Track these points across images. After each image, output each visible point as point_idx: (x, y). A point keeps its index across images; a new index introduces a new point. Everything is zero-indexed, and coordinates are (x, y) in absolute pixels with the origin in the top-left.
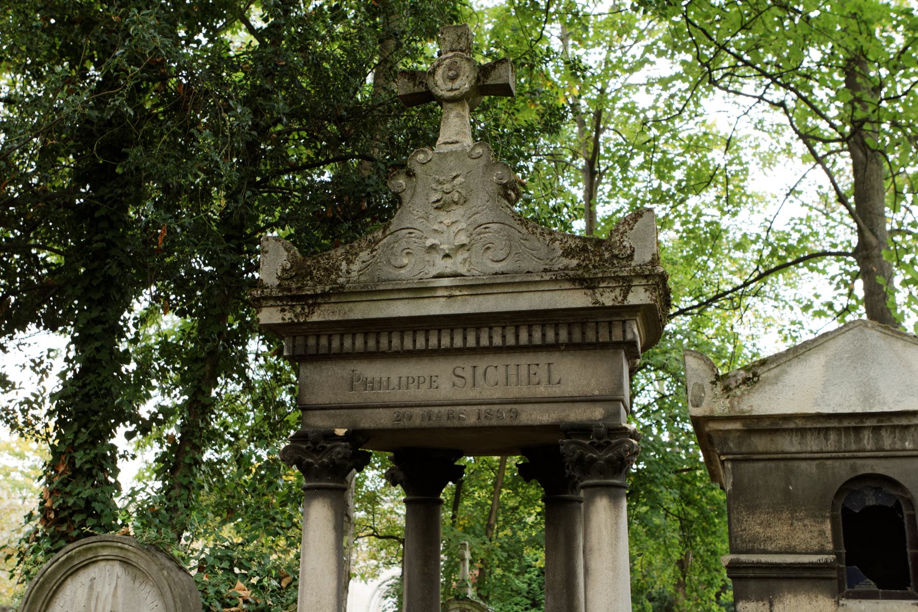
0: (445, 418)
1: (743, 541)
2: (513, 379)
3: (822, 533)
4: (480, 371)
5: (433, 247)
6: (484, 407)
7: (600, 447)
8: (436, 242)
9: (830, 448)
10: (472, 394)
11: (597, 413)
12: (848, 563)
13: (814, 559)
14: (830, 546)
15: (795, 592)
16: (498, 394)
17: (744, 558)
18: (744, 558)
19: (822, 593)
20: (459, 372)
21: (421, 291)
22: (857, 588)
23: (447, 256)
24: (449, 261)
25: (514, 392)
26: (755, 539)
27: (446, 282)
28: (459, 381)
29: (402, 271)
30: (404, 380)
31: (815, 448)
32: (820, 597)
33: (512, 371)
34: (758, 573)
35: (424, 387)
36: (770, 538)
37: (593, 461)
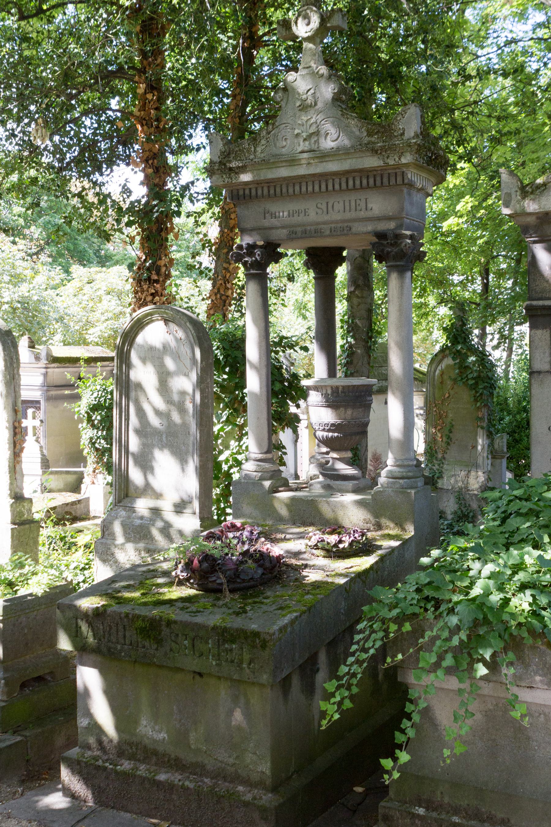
1: (536, 292)
2: (347, 208)
4: (330, 205)
5: (298, 135)
6: (333, 226)
8: (300, 131)
10: (326, 218)
11: (392, 225)
16: (338, 217)
17: (535, 303)
18: (535, 303)
20: (319, 205)
21: (292, 162)
23: (305, 140)
24: (307, 143)
25: (348, 215)
27: (305, 155)
28: (319, 211)
33: (347, 204)
34: (545, 312)
35: (302, 215)
37: (388, 253)
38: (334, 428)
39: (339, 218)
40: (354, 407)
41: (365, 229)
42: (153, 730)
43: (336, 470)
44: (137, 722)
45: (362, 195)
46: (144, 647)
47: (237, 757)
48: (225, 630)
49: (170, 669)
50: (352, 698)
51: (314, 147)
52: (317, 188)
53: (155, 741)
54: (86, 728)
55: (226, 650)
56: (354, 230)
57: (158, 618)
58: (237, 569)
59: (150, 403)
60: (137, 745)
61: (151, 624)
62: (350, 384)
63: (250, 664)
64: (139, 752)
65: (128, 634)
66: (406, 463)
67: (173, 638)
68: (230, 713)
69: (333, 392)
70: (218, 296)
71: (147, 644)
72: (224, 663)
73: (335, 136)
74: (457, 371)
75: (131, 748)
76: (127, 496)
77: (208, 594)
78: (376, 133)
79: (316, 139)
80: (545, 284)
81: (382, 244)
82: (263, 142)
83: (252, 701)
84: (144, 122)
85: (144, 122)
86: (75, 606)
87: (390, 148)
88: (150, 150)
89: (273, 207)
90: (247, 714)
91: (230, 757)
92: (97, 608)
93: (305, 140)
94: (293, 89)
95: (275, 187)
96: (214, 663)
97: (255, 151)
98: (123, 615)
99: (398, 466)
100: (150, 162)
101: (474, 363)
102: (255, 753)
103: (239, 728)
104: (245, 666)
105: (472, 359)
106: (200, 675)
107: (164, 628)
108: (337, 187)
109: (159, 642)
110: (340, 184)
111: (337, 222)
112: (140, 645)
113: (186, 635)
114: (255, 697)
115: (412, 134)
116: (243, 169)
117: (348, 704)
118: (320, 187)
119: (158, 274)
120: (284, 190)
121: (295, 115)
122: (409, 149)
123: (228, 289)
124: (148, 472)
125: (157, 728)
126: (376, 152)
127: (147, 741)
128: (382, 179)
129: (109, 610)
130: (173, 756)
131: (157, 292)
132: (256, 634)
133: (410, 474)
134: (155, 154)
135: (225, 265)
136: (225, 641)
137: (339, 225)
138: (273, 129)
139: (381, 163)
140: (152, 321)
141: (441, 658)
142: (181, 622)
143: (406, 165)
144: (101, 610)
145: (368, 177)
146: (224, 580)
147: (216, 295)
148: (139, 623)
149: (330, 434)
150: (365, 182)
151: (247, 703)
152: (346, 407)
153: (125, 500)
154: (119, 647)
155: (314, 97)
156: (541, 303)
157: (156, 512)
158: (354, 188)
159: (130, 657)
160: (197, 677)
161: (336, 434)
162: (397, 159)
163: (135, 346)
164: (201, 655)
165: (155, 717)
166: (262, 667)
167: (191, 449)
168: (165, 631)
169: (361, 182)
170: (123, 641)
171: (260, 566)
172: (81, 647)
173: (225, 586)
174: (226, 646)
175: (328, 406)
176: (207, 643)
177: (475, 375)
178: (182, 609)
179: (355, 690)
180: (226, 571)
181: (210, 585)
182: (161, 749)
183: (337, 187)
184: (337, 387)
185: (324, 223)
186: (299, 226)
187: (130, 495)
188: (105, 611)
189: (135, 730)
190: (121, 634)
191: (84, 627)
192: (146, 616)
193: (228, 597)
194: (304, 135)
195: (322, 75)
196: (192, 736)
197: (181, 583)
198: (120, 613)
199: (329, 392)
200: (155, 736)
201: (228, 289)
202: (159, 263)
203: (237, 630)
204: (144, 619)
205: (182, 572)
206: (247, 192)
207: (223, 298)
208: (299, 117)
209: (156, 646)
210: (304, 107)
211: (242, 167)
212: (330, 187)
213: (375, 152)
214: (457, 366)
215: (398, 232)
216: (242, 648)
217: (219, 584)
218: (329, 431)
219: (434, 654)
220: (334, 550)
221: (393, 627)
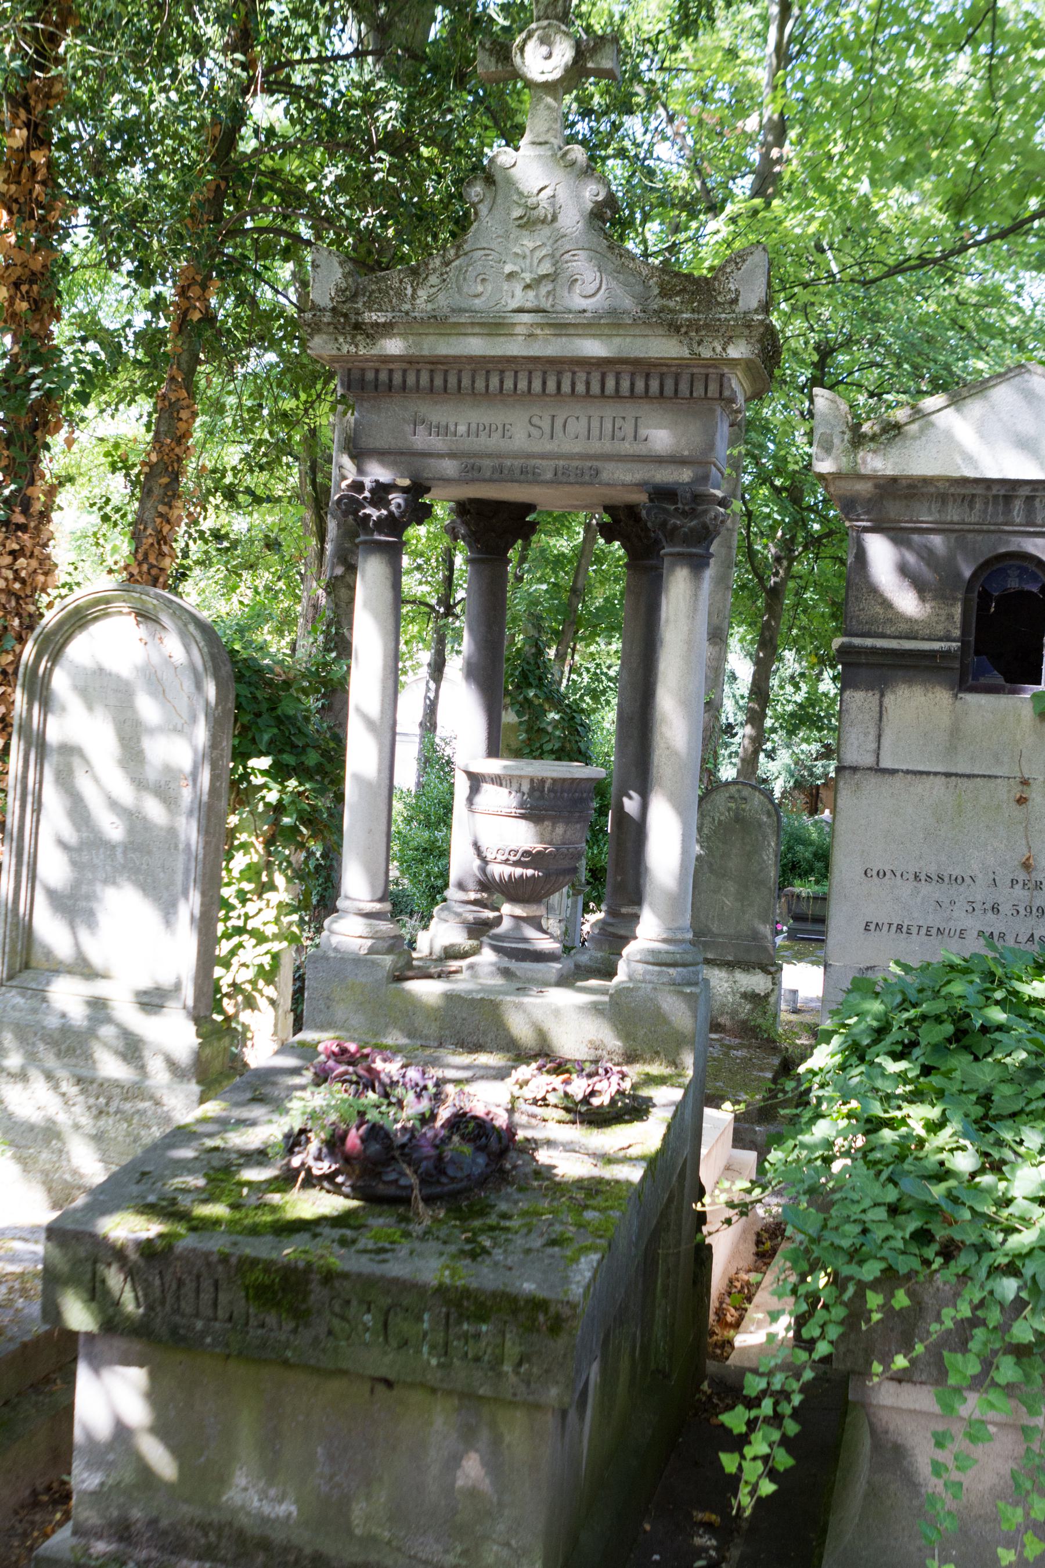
0: (517, 472)
1: (859, 622)
2: (595, 432)
3: (950, 617)
5: (511, 275)
6: (561, 463)
7: (684, 514)
8: (516, 269)
9: (973, 519)
10: (549, 447)
11: (685, 475)
12: (977, 653)
13: (936, 646)
14: (957, 633)
15: (910, 682)
16: (577, 448)
17: (857, 641)
18: (857, 641)
19: (940, 683)
20: (536, 420)
22: (983, 680)
23: (528, 287)
24: (531, 294)
25: (596, 446)
26: (873, 620)
27: (526, 318)
28: (535, 432)
29: (477, 301)
30: (474, 426)
31: (956, 518)
32: (938, 689)
33: (595, 424)
35: (496, 436)
36: (890, 620)
37: (675, 528)
38: (530, 859)
39: (576, 450)
40: (568, 822)
41: (628, 478)
42: (263, 1495)
43: (526, 940)
44: (223, 1480)
45: (629, 410)
46: (262, 1325)
47: (465, 1553)
48: (466, 1293)
49: (316, 1371)
50: (785, 1442)
51: (547, 304)
52: (537, 385)
53: (265, 1520)
54: (93, 1493)
55: (465, 1337)
56: (605, 476)
57: (301, 1265)
58: (440, 1158)
59: (96, 780)
60: (220, 1529)
61: (285, 1279)
62: (568, 776)
63: (520, 1364)
64: (224, 1542)
65: (223, 1298)
66: (679, 936)
67: (337, 1309)
68: (454, 1462)
69: (532, 789)
70: (145, 567)
71: (271, 1319)
72: (457, 1362)
73: (591, 288)
74: (523, 736)
75: (206, 1535)
76: (26, 966)
77: (377, 1209)
78: (678, 293)
79: (550, 287)
80: (878, 609)
81: (666, 511)
82: (433, 279)
83: (507, 1439)
84: (15, 207)
85: (15, 207)
86: (93, 1236)
87: (707, 326)
88: (24, 265)
89: (439, 413)
90: (494, 1465)
91: (446, 1551)
92: (149, 1241)
93: (528, 287)
94: (510, 182)
95: (446, 372)
96: (434, 1362)
97: (414, 297)
98: (214, 1258)
99: (665, 941)
100: (24, 288)
101: (556, 724)
102: (508, 1544)
103: (472, 1493)
104: (507, 1368)
105: (553, 716)
106: (389, 1384)
107: (315, 1286)
108: (581, 388)
109: (301, 1316)
110: (588, 384)
111: (570, 457)
112: (253, 1322)
113: (369, 1304)
114: (516, 1433)
115: (755, 304)
116: (386, 329)
117: (784, 1460)
118: (544, 383)
119: (25, 512)
120: (466, 382)
121: (506, 235)
122: (746, 332)
123: (164, 555)
124: (78, 920)
125: (272, 1492)
126: (677, 329)
127: (243, 1520)
128: (676, 384)
129: (180, 1246)
130: (308, 1551)
131: (22, 549)
132: (538, 1305)
133: (689, 958)
134: (33, 274)
135: (162, 509)
136: (462, 1317)
137: (575, 463)
138: (457, 256)
139: (685, 353)
140: (107, 615)
141: (988, 1364)
142: (359, 1275)
143: (733, 362)
144: (160, 1245)
145: (647, 376)
146: (414, 1180)
147: (140, 564)
148: (257, 1276)
149: (518, 871)
150: (640, 385)
151: (497, 1441)
152: (555, 820)
153: (25, 975)
154: (199, 1325)
155: (553, 204)
156: (869, 642)
157: (98, 1006)
158: (617, 395)
159: (227, 1345)
160: (380, 1388)
161: (530, 872)
162: (719, 349)
163: (64, 661)
164: (404, 1343)
165: (271, 1471)
166: (547, 1371)
167: (179, 878)
168: (317, 1293)
169: (632, 385)
170: (209, 1313)
171: (480, 1149)
172: (112, 1323)
173: (416, 1192)
174: (465, 1326)
175: (522, 817)
176: (419, 1319)
177: (557, 746)
178: (343, 1242)
179: (792, 1428)
180: (421, 1160)
181: (382, 1189)
182: (278, 1536)
183: (581, 388)
184: (543, 781)
185: (543, 456)
186: (489, 456)
187: (33, 964)
188: (170, 1247)
189: (219, 1495)
190: (206, 1297)
191: (115, 1279)
192: (272, 1262)
193: (426, 1216)
194: (528, 277)
195: (573, 163)
196: (358, 1511)
197: (311, 1181)
198: (207, 1255)
199: (526, 788)
200: (266, 1509)
201: (164, 555)
202: (29, 491)
203: (494, 1294)
204: (268, 1266)
205: (319, 1158)
206: (383, 376)
207: (154, 571)
208: (517, 239)
209: (292, 1325)
210: (529, 222)
211: (384, 325)
212: (566, 388)
213: (674, 328)
214: (523, 727)
215: (701, 489)
216: (503, 1334)
217: (405, 1187)
218: (517, 864)
219: (971, 1357)
220: (583, 1109)
221: (874, 1300)
